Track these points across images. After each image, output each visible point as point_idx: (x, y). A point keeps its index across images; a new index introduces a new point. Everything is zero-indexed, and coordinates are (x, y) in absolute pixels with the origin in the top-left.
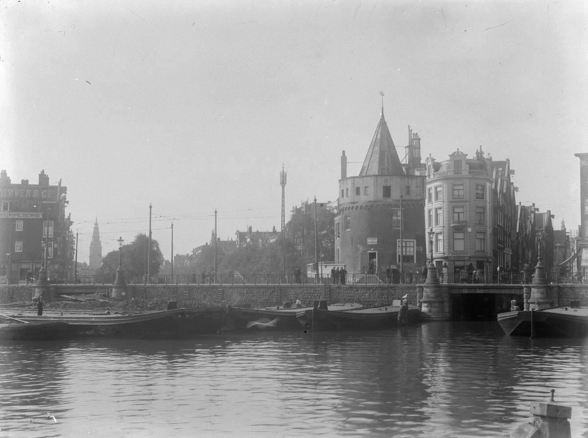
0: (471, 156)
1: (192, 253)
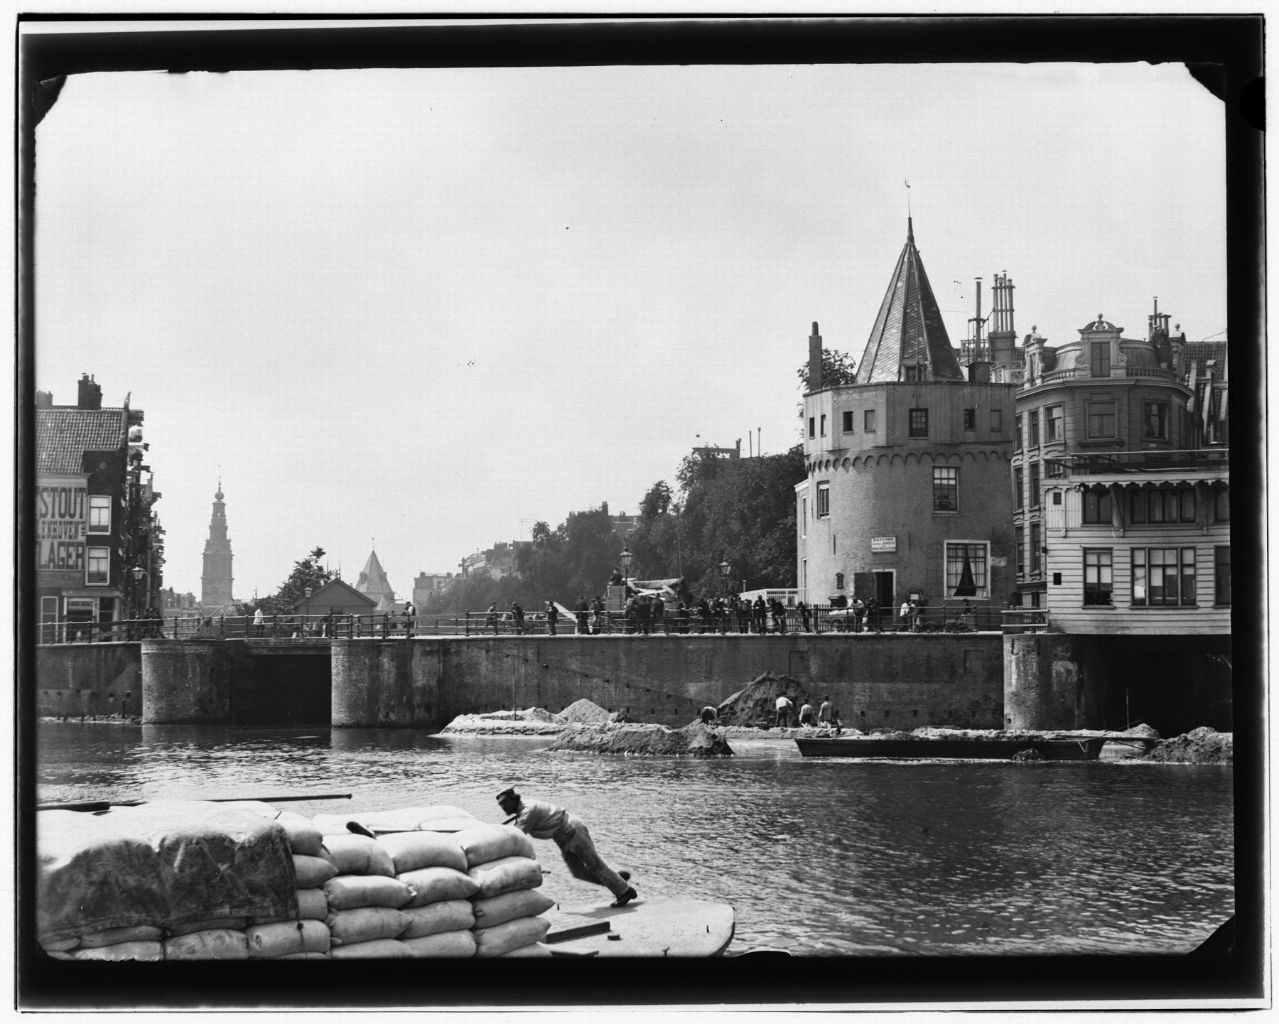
0: (1138, 331)
1: (460, 570)
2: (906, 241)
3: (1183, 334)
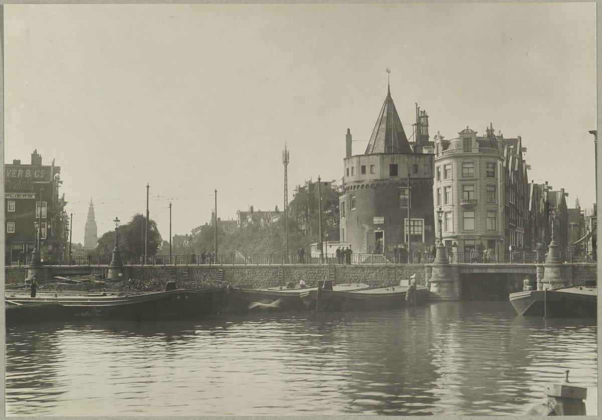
3: (502, 135)
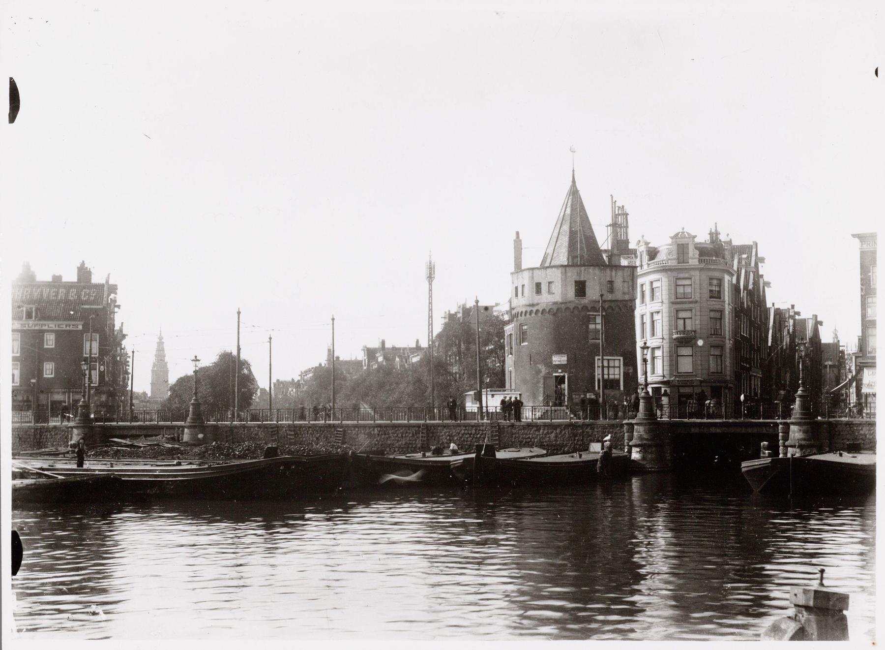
2: (571, 184)
